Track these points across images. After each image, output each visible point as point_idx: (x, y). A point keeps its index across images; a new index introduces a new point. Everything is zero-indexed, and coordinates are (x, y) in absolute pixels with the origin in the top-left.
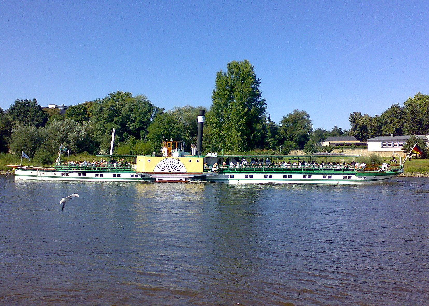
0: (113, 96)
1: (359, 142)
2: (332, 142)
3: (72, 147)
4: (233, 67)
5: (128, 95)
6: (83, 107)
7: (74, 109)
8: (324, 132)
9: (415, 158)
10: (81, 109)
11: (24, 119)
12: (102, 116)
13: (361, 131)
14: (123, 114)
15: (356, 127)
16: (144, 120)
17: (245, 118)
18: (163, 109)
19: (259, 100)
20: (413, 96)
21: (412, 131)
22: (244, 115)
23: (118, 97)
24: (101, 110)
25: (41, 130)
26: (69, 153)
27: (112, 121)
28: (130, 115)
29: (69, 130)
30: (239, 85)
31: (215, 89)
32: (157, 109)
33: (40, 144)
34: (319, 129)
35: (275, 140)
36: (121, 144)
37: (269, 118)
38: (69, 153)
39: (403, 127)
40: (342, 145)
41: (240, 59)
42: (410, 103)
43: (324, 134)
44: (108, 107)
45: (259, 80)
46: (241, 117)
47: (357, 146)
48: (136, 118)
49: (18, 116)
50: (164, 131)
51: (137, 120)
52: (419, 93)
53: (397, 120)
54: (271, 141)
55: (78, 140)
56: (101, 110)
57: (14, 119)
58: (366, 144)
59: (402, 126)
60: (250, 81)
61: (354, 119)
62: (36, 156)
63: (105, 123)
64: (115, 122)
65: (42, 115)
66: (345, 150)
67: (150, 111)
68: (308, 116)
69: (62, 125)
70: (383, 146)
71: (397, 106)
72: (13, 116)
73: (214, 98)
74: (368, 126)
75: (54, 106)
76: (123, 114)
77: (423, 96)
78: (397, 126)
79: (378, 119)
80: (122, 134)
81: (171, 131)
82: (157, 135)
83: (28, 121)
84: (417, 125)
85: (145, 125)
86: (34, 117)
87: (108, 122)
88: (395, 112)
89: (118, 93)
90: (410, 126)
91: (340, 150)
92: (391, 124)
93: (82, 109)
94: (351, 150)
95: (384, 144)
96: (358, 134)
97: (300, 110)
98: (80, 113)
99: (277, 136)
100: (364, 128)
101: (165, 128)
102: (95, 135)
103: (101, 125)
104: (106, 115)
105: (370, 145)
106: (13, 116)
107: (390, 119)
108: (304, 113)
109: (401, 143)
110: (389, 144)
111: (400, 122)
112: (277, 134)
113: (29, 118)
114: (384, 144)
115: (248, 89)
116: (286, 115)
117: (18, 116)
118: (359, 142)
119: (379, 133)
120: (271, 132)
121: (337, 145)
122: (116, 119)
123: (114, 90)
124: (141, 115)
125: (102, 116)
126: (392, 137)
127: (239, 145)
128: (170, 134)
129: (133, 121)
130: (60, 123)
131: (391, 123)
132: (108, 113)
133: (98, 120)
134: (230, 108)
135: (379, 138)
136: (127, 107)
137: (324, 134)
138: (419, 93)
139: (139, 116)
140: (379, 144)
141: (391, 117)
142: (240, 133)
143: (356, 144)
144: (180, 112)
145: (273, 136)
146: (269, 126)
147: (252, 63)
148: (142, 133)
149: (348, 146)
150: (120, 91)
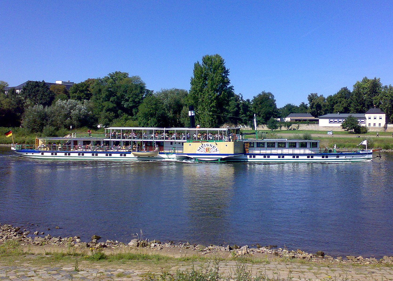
0: (112, 76)
1: (313, 118)
2: (292, 118)
3: (75, 123)
4: (207, 60)
5: (125, 75)
6: (85, 85)
7: (78, 86)
8: (293, 107)
9: (351, 133)
10: (83, 87)
11: (34, 98)
12: (101, 96)
13: (317, 109)
14: (119, 94)
15: (313, 106)
16: (137, 100)
17: (215, 101)
18: (152, 91)
19: (228, 87)
20: (360, 80)
21: (357, 109)
22: (215, 99)
23: (116, 77)
24: (100, 90)
25: (48, 110)
26: (71, 128)
27: (109, 101)
28: (124, 95)
29: (71, 108)
30: (211, 74)
31: (193, 77)
32: (148, 91)
33: (47, 120)
34: (290, 105)
35: (246, 116)
36: (115, 120)
37: (242, 98)
38: (71, 128)
39: (350, 106)
40: (300, 120)
41: (212, 53)
42: (358, 86)
43: (293, 109)
44: (105, 88)
45: (228, 70)
46: (212, 101)
47: (311, 122)
48: (129, 98)
49: (29, 95)
50: (151, 110)
51: (130, 100)
52: (366, 78)
53: (345, 100)
54: (243, 117)
55: (80, 117)
56: (100, 90)
57: (26, 98)
58: (318, 120)
59: (349, 105)
60: (220, 71)
61: (311, 98)
62: (44, 131)
63: (102, 102)
64: (111, 101)
65: (49, 95)
66: (301, 125)
67: (142, 93)
68: (273, 96)
69: (66, 104)
70: (330, 122)
71: (345, 89)
72: (24, 95)
73: (192, 84)
74: (322, 105)
75: (60, 82)
76: (119, 94)
77: (368, 80)
78: (345, 105)
79: (331, 98)
80: (118, 111)
81: (157, 110)
82: (145, 113)
83: (38, 100)
84: (360, 105)
85: (137, 104)
86: (42, 96)
87: (106, 101)
88: (344, 93)
89: (116, 73)
90: (355, 105)
91: (297, 125)
92: (340, 103)
93: (85, 87)
94: (306, 124)
95: (331, 120)
96: (314, 111)
97: (267, 92)
98: (83, 91)
99: (248, 113)
100: (319, 107)
101: (152, 108)
102: (94, 112)
103: (100, 103)
104: (104, 95)
105: (320, 120)
106: (24, 95)
107: (339, 100)
108: (270, 94)
109: (340, 120)
110: (335, 120)
111: (347, 102)
112: (248, 111)
113: (38, 98)
114: (331, 120)
115: (218, 78)
116: (256, 95)
117: (29, 95)
118: (313, 118)
119: (332, 111)
120: (243, 109)
121: (296, 120)
122: (112, 99)
123: (113, 71)
124: (134, 96)
125: (101, 96)
126: (338, 115)
127: (209, 124)
128: (156, 113)
129: (127, 100)
130: (64, 102)
131: (340, 102)
132: (105, 94)
133: (97, 99)
134: (204, 93)
135: (329, 115)
136: (122, 89)
137: (293, 109)
138: (366, 78)
139: (132, 97)
140: (328, 120)
141: (340, 98)
142: (211, 113)
143: (311, 120)
144: (166, 94)
145: (245, 113)
146: (241, 105)
147: (223, 57)
148: (134, 111)
149: (304, 122)
150: (118, 71)
